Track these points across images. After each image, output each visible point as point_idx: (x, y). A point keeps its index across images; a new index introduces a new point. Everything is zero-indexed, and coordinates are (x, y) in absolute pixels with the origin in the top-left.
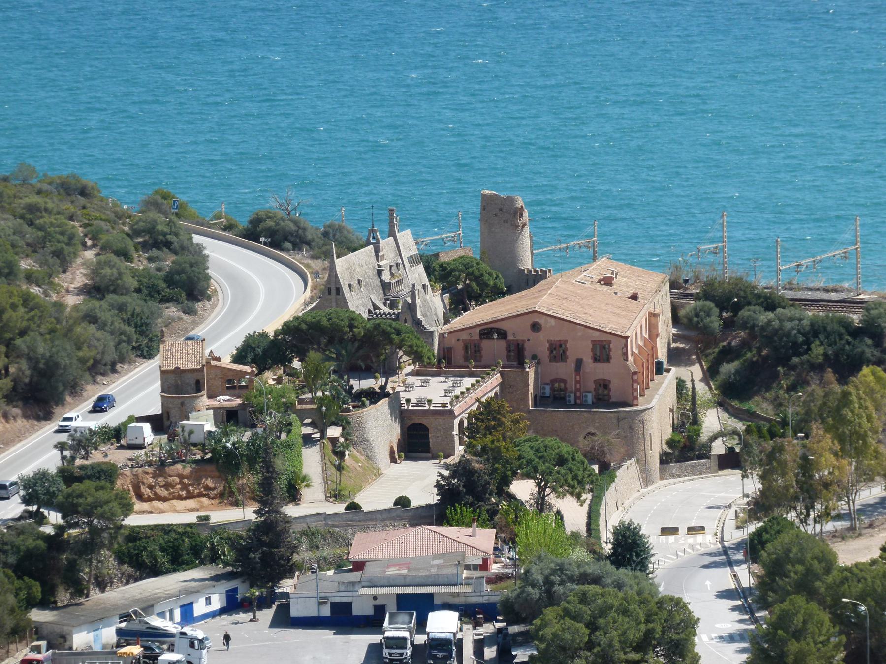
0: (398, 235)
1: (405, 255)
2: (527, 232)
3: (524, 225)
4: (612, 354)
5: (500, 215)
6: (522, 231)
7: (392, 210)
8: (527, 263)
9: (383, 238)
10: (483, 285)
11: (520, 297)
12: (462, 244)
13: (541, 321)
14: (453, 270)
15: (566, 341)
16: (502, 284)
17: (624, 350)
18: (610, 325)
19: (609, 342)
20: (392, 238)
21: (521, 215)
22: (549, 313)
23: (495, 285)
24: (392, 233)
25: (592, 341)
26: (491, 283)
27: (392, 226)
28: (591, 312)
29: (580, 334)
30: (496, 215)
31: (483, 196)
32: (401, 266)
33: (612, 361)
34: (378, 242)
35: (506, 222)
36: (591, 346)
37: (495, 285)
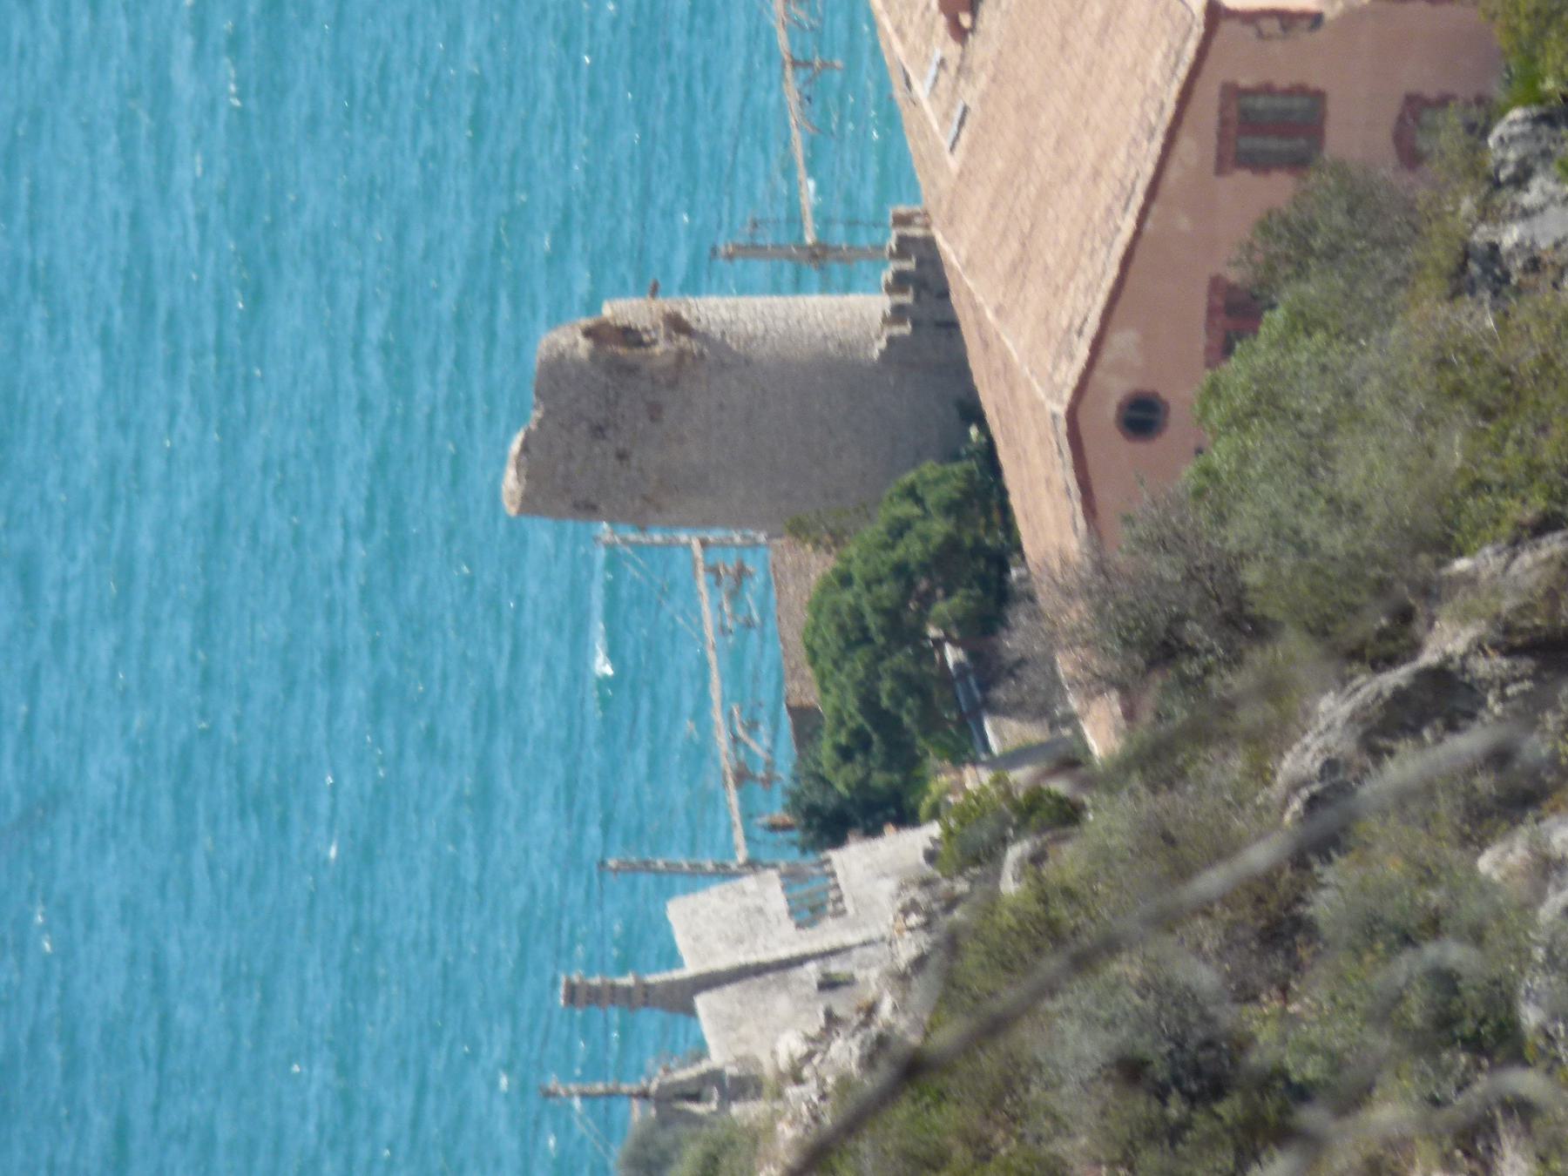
0: (691, 968)
1: (783, 941)
2: (712, 310)
3: (677, 325)
4: (1282, 81)
5: (623, 426)
6: (705, 337)
7: (572, 993)
8: (859, 313)
9: (701, 1052)
10: (948, 562)
11: (1007, 444)
12: (738, 617)
13: (1115, 389)
14: (869, 703)
15: (1216, 284)
16: (943, 479)
17: (1272, 26)
18: (1155, 75)
19: (1231, 92)
20: (702, 1002)
21: (629, 335)
22: (1083, 351)
23: (951, 508)
24: (680, 999)
25: (1221, 168)
26: (940, 527)
27: (646, 996)
28: (1089, 148)
29: (1184, 223)
30: (622, 456)
31: (528, 505)
32: (835, 967)
33: (1315, 81)
34: (715, 1077)
35: (655, 412)
36: (1243, 177)
37: (951, 508)
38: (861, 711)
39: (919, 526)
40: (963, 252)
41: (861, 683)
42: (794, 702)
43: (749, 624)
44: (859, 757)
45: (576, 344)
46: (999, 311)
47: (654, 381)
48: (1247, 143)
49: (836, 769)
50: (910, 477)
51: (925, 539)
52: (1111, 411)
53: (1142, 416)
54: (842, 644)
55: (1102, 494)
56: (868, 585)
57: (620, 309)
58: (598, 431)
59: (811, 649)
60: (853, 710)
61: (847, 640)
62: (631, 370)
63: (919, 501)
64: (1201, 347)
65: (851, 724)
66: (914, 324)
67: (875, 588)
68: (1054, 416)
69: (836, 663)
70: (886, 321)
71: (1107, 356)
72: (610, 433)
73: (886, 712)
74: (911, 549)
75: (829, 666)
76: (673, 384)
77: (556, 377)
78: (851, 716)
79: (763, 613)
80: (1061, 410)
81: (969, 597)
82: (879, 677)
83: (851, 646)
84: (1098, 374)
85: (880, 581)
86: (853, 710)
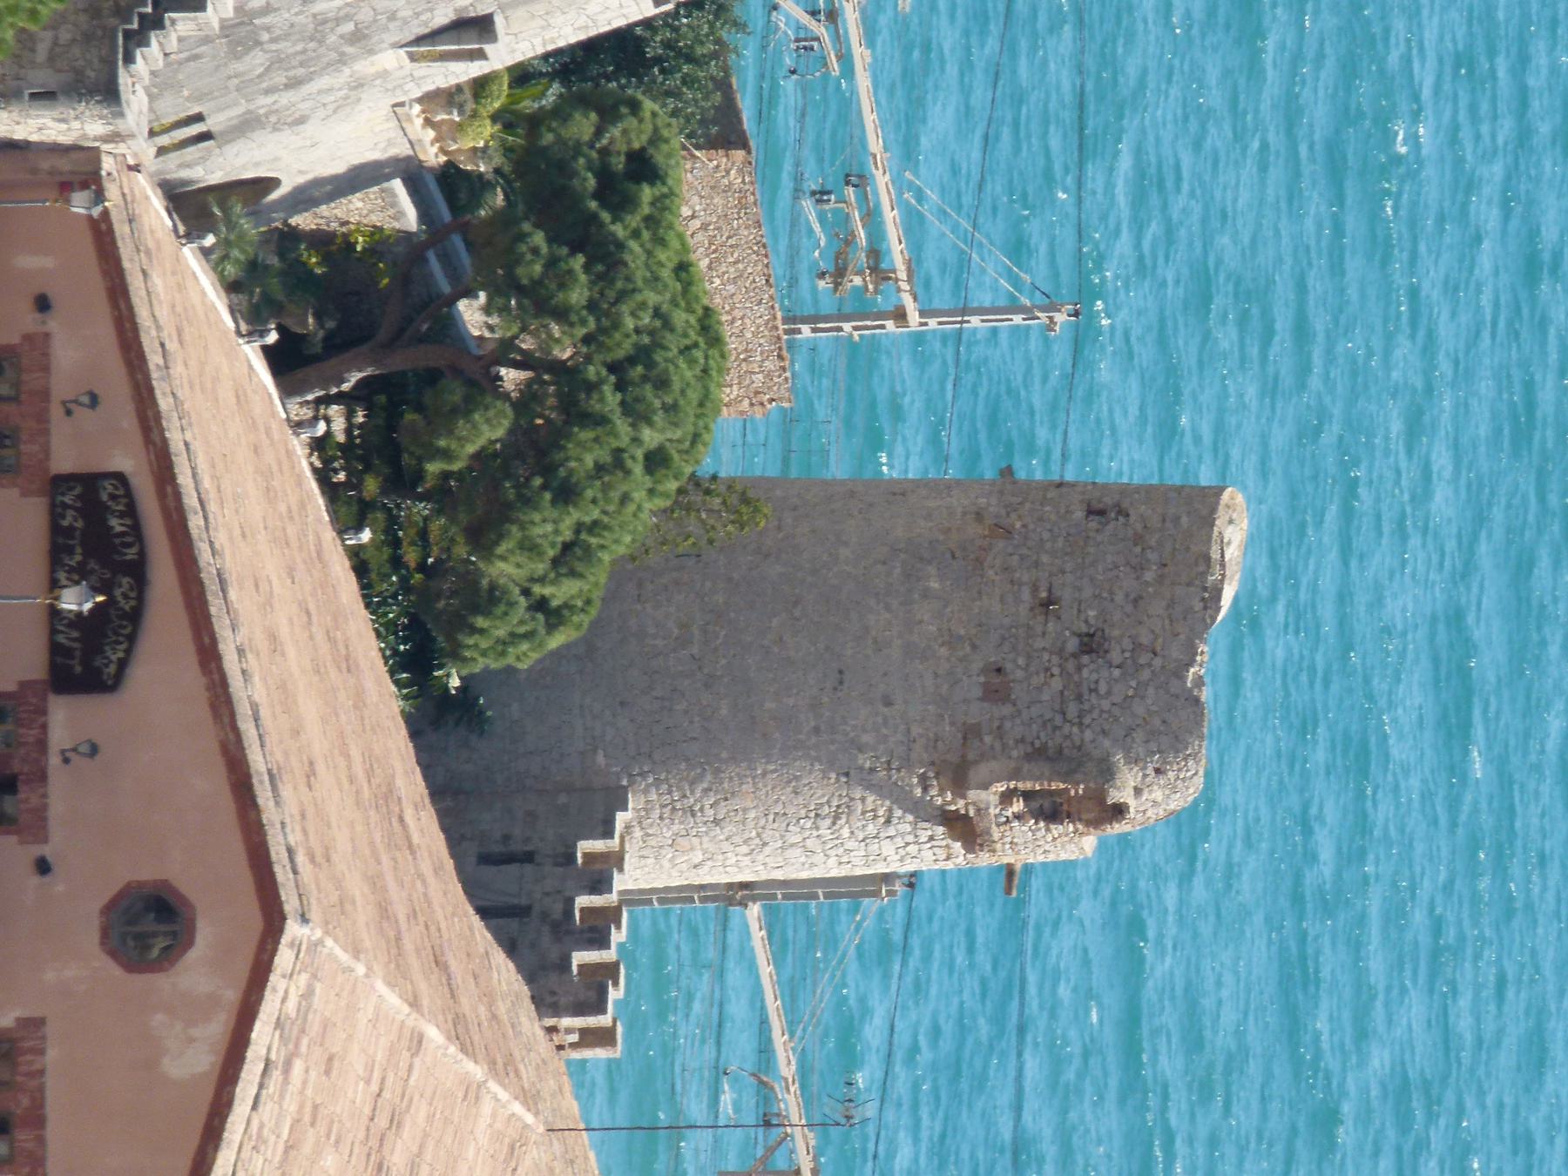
2: (911, 849)
3: (965, 829)
5: (1047, 639)
6: (923, 812)
8: (659, 851)
13: (201, 972)
14: (606, 259)
21: (1050, 811)
23: (489, 600)
26: (505, 569)
35: (997, 687)
37: (489, 600)
38: (621, 246)
39: (541, 567)
40: (487, 1107)
41: (622, 296)
42: (739, 154)
43: (820, 195)
44: (619, 163)
45: (1138, 791)
46: (418, 1040)
47: (1000, 732)
48: (164, 140)
49: (656, 139)
50: (556, 641)
51: (530, 547)
52: (205, 935)
53: (149, 924)
54: (658, 357)
55: (213, 784)
56: (618, 460)
57: (1073, 845)
58: (1091, 644)
59: (715, 341)
60: (633, 245)
61: (650, 365)
62: (1038, 754)
63: (541, 605)
64: (52, 1054)
65: (634, 220)
66: (571, 858)
67: (606, 458)
68: (304, 919)
69: (667, 324)
70: (617, 859)
71: (217, 1028)
72: (1072, 645)
73: (575, 249)
74: (549, 525)
75: (680, 317)
76: (970, 733)
77: (1171, 726)
78: (636, 234)
79: (795, 220)
80: (293, 929)
81: (447, 455)
82: (592, 306)
83: (643, 355)
84: (232, 995)
85: (600, 469)
86: (633, 245)
